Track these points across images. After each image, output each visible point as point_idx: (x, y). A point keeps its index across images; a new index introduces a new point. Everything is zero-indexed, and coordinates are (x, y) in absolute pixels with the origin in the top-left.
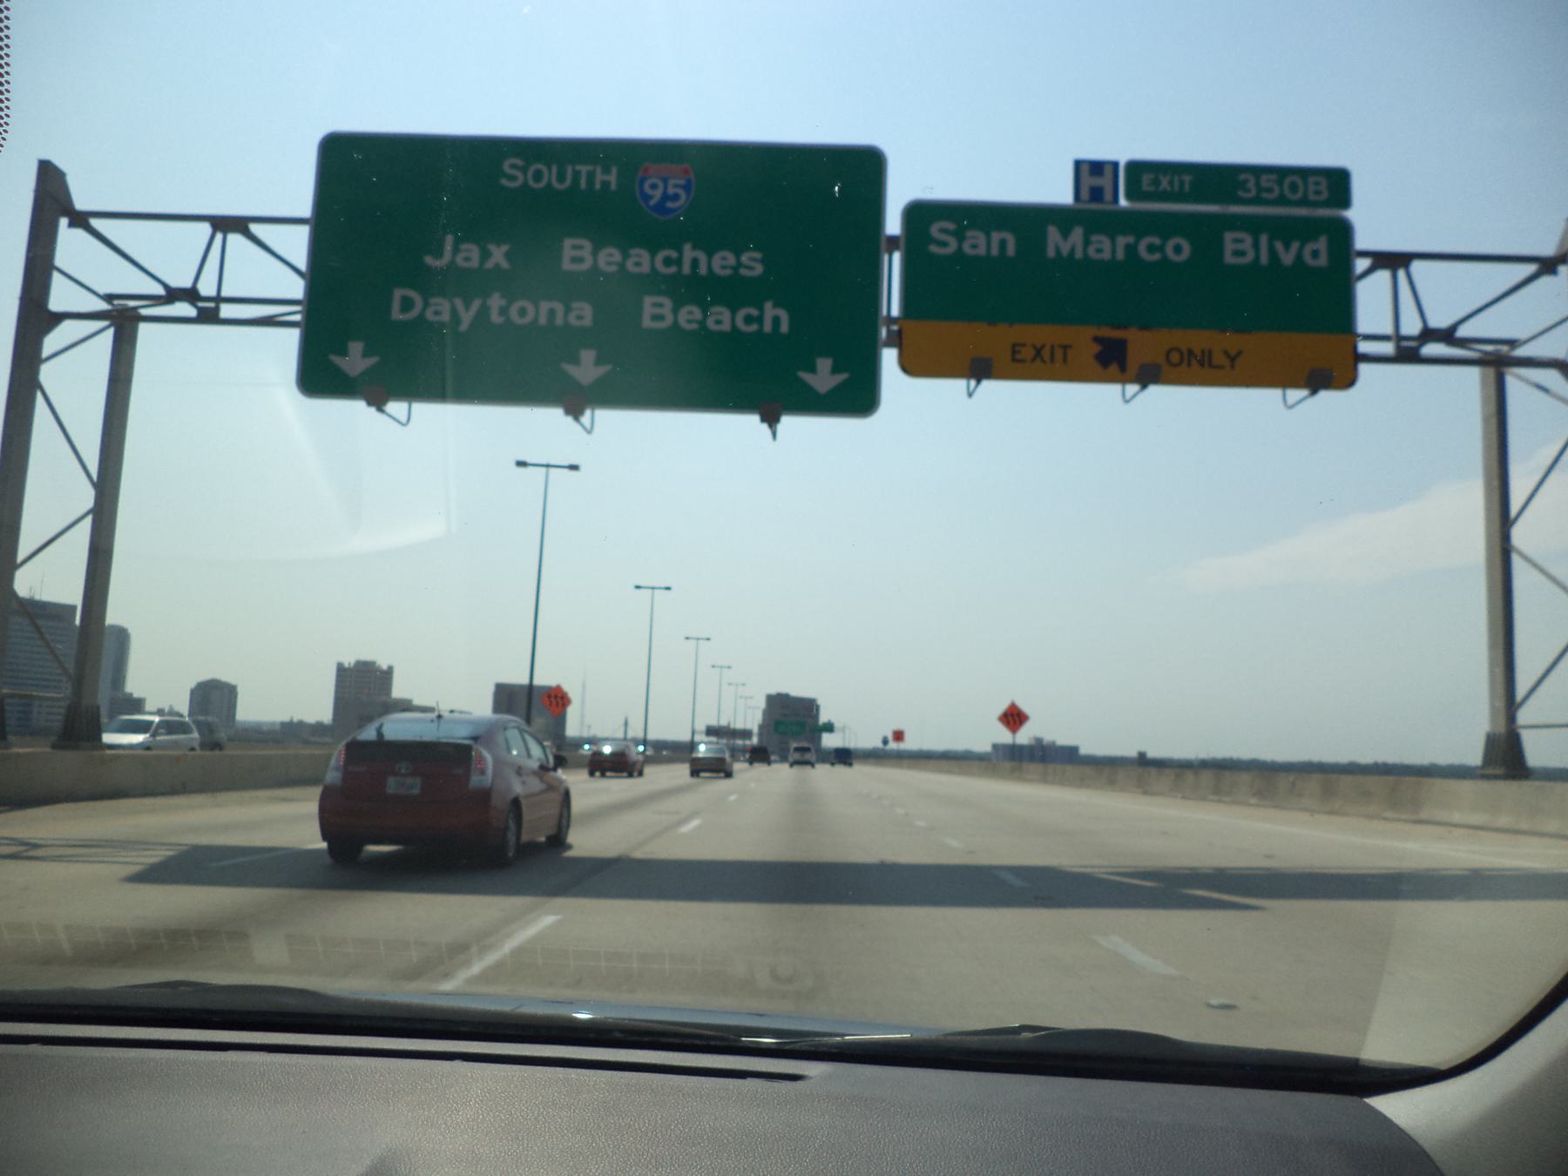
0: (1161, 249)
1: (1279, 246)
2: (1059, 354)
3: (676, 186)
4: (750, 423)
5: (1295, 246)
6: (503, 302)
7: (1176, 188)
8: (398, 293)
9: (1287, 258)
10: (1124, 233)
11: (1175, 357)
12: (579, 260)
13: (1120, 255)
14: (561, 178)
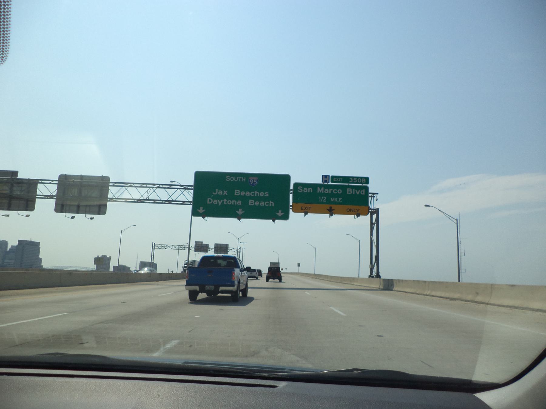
0: (337, 191)
1: (356, 191)
5: (359, 191)
6: (226, 201)
7: (339, 180)
9: (358, 193)
11: (348, 210)
13: (330, 192)
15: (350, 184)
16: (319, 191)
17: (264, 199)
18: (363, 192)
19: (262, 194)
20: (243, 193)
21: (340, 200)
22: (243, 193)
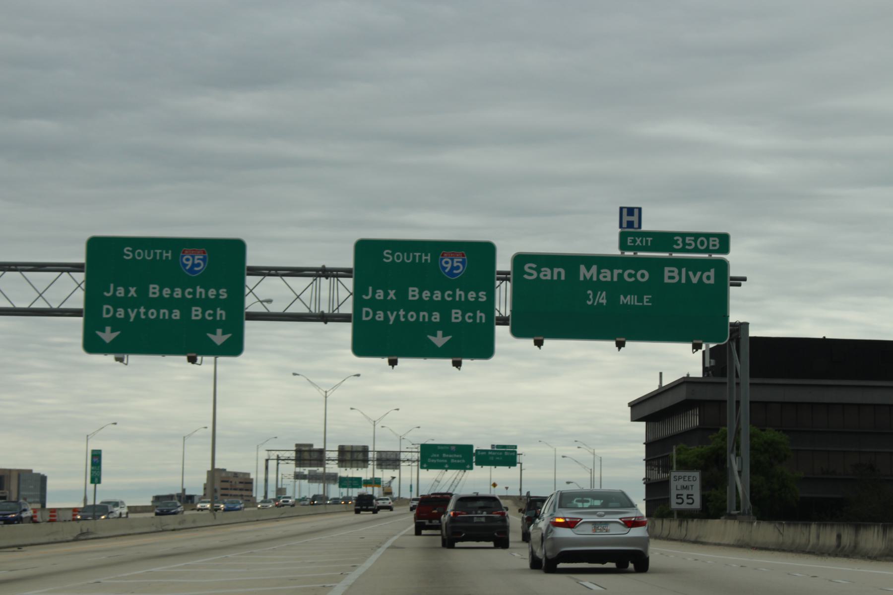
0: (635, 276)
1: (691, 273)
2: (690, 487)
3: (457, 262)
4: (827, 337)
5: (699, 274)
8: (105, 307)
9: (695, 280)
10: (618, 269)
12: (673, 278)
13: (615, 279)
14: (408, 259)
15: (675, 255)
16: (584, 275)
17: (459, 459)
18: (708, 278)
19: (458, 456)
20: (447, 456)
21: (645, 300)
22: (447, 456)
